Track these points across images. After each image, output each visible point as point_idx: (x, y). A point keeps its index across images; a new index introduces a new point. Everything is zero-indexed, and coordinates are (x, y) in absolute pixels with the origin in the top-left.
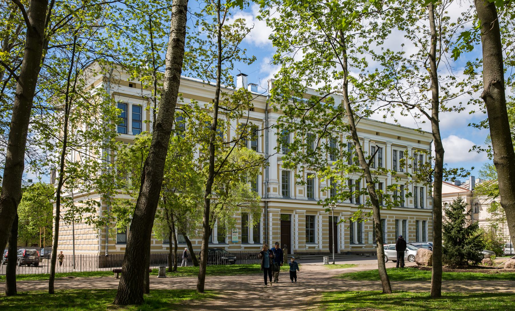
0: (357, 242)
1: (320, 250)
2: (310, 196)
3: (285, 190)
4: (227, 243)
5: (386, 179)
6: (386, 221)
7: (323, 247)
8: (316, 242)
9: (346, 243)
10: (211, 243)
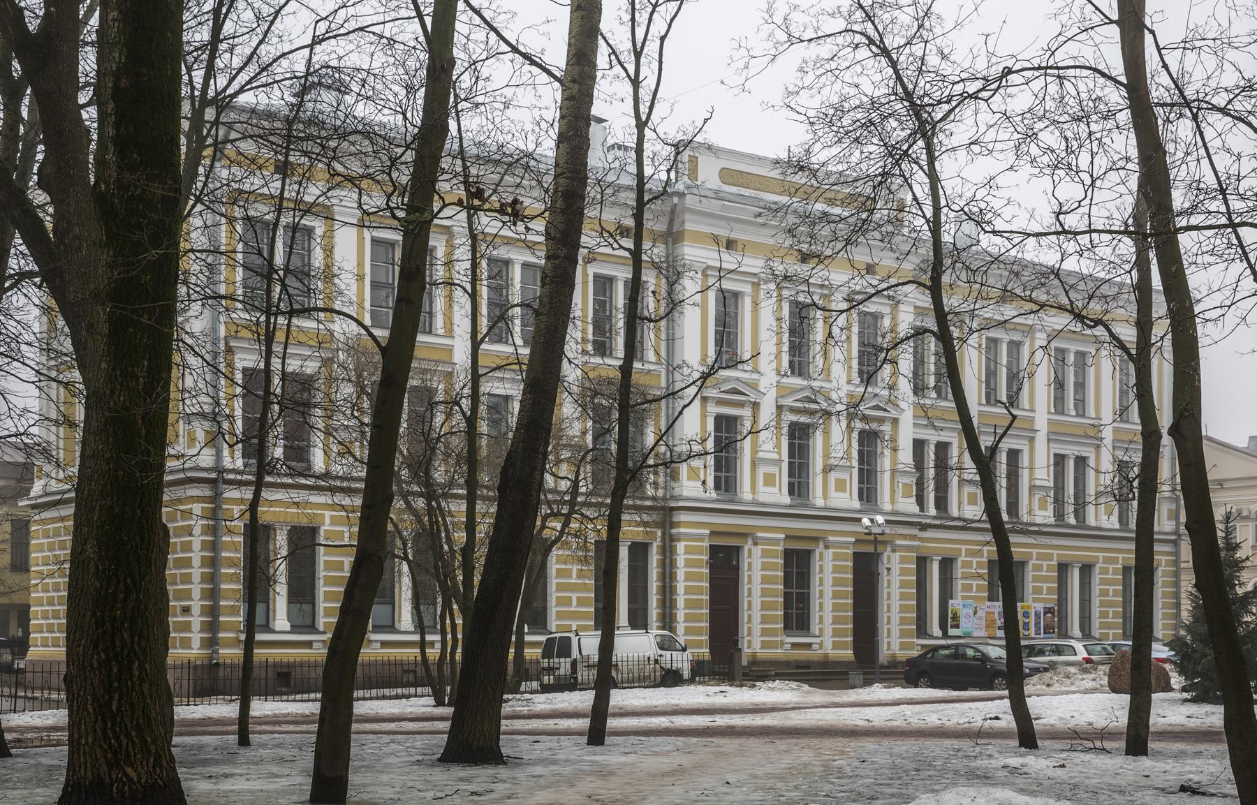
0: (937, 631)
1: (826, 655)
2: (798, 485)
3: (796, 480)
4: (321, 628)
5: (1032, 439)
6: (1097, 569)
7: (836, 646)
8: (815, 628)
9: (903, 634)
10: (267, 628)
